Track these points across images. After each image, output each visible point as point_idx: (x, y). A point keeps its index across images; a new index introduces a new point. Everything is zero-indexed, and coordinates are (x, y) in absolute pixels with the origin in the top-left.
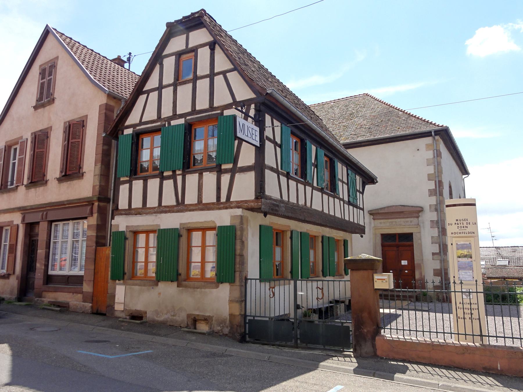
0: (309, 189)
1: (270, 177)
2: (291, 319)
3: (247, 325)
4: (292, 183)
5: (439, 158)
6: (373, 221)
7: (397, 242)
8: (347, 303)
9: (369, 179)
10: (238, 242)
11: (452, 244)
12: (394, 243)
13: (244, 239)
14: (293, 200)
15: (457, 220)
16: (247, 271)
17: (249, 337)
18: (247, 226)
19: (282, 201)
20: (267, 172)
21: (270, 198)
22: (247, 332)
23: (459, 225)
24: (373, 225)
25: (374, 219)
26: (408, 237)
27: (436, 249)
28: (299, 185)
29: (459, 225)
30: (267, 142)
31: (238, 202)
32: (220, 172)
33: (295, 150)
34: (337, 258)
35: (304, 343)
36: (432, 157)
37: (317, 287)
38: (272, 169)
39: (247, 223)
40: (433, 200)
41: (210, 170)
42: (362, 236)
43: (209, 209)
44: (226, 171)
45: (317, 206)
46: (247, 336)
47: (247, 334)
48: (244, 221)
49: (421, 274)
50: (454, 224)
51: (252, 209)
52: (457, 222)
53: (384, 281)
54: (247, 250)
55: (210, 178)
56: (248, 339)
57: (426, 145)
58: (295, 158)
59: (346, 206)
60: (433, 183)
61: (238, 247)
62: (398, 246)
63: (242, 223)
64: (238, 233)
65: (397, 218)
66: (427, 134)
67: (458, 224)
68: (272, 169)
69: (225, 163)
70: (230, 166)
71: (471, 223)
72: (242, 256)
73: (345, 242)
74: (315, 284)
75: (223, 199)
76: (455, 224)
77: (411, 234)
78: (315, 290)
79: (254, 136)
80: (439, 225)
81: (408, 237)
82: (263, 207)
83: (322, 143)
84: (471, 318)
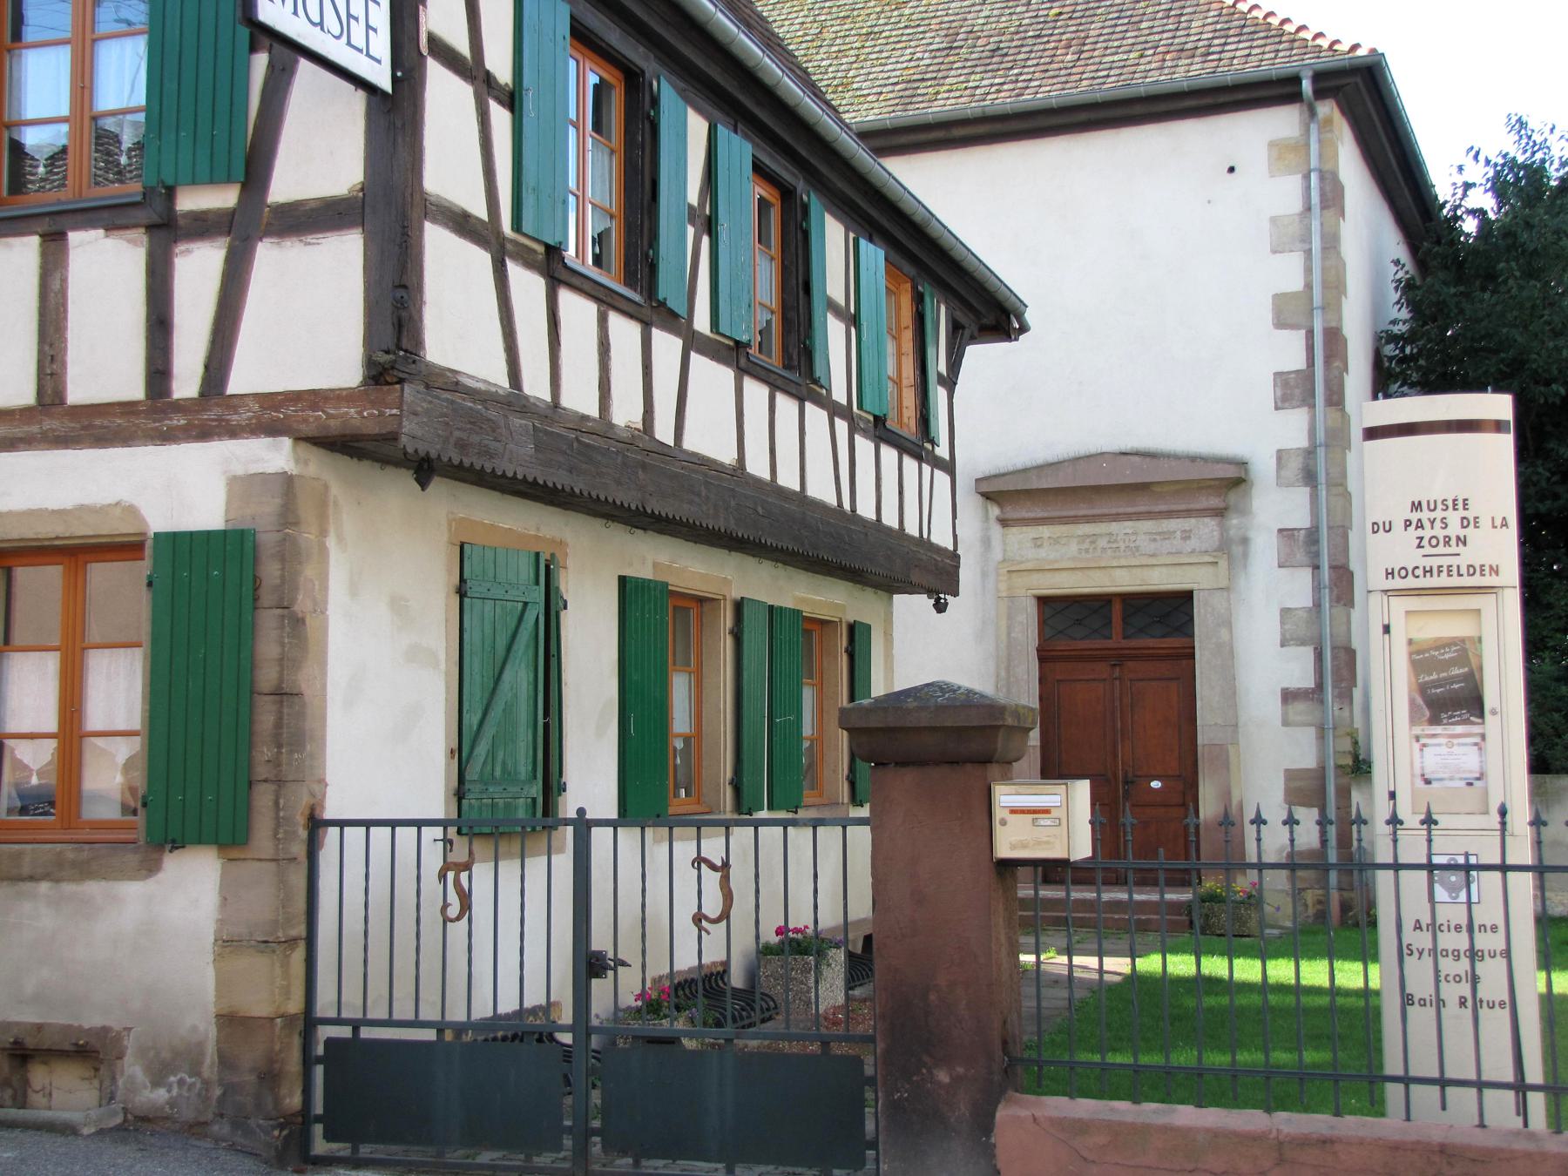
0: (667, 346)
1: (453, 273)
2: (563, 1029)
3: (319, 1071)
4: (577, 311)
5: (1329, 213)
6: (996, 531)
7: (1116, 641)
8: (858, 948)
9: (991, 314)
10: (268, 621)
11: (1387, 629)
12: (1098, 643)
13: (302, 604)
14: (580, 398)
15: (1416, 506)
16: (323, 782)
17: (329, 1136)
18: (323, 533)
19: (515, 401)
20: (437, 242)
21: (446, 383)
22: (319, 1109)
23: (1427, 533)
24: (997, 554)
25: (1004, 522)
26: (1170, 613)
27: (1298, 669)
28: (616, 321)
29: (1427, 533)
30: (437, 76)
31: (270, 401)
32: (166, 231)
33: (598, 127)
34: (816, 714)
35: (624, 1153)
36: (1297, 206)
37: (699, 861)
38: (461, 223)
39: (323, 518)
40: (1293, 429)
41: (110, 217)
42: (940, 607)
43: (103, 439)
44: (204, 226)
45: (709, 437)
46: (318, 1129)
47: (318, 1119)
48: (306, 511)
49: (1227, 794)
50: (1398, 525)
51: (343, 445)
52: (1414, 517)
53: (1046, 818)
54: (323, 664)
55: (106, 266)
56: (320, 1146)
57: (1272, 145)
58: (588, 178)
59: (864, 446)
60: (1296, 339)
61: (268, 647)
62: (1119, 658)
63: (288, 516)
64: (270, 571)
65: (1116, 517)
66: (1273, 91)
67: (1420, 525)
68: (461, 223)
69: (194, 182)
70: (224, 198)
71: (1485, 522)
72: (285, 695)
73: (857, 636)
74: (685, 850)
75: (186, 382)
76: (1408, 523)
77: (1184, 599)
78: (686, 876)
79: (358, 31)
80: (1317, 555)
81: (1170, 613)
82: (408, 426)
83: (748, 100)
84: (1474, 1004)
